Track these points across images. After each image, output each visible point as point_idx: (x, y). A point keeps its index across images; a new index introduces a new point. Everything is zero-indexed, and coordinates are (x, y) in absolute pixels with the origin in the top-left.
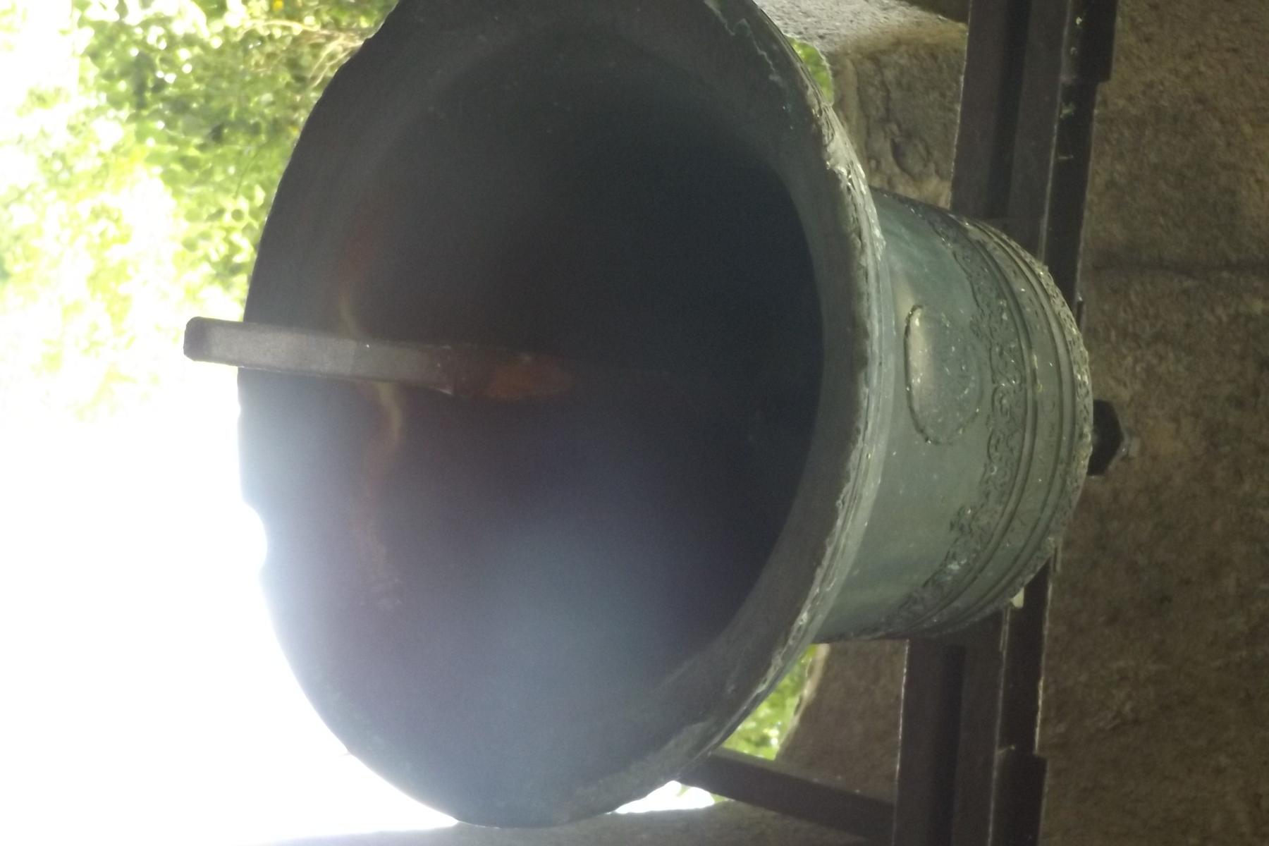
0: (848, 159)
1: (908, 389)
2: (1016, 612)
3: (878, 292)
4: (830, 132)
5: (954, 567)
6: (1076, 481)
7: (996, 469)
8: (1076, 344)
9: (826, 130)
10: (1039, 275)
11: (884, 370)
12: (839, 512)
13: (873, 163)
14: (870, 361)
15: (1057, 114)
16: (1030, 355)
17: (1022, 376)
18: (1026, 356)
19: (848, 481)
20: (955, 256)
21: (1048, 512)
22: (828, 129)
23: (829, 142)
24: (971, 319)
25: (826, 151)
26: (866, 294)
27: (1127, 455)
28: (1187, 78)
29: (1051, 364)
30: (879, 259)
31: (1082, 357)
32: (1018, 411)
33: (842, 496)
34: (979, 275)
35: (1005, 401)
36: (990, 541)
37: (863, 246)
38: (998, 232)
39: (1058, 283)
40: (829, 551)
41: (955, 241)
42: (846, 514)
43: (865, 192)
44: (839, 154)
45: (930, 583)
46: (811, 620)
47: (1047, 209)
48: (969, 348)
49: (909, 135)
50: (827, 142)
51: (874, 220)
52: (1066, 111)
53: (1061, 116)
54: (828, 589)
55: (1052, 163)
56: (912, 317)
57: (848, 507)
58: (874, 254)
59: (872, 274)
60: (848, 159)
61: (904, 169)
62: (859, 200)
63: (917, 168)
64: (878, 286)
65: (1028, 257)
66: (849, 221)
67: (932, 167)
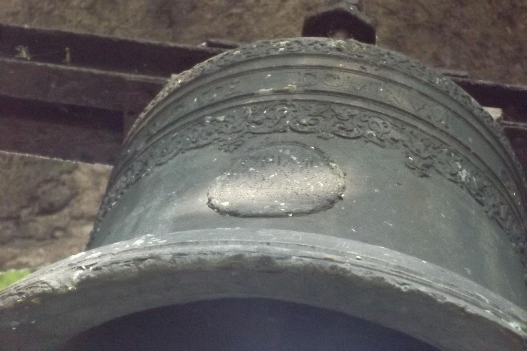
0: (67, 269)
1: (291, 215)
2: (505, 116)
3: (197, 243)
4: (40, 285)
5: (464, 175)
6: (382, 55)
7: (369, 132)
8: (249, 51)
9: (39, 289)
10: (181, 84)
11: (274, 240)
12: (412, 288)
13: (58, 234)
14: (265, 254)
15: (28, 62)
16: (258, 95)
17: (280, 104)
18: (261, 100)
19: (382, 278)
20: (160, 165)
21: (410, 82)
22: (37, 287)
23: (50, 286)
24: (222, 151)
25: (57, 290)
26: (199, 255)
27: (356, 5)
28: (347, 84)
29: (269, 75)
30: (165, 241)
31: (262, 46)
32: (314, 108)
33: (397, 286)
34: (179, 142)
35: (304, 121)
36: (439, 139)
37: (152, 257)
38: (137, 121)
39: (189, 66)
40: (450, 299)
41: (146, 164)
42: (417, 282)
43: (99, 253)
44: (61, 277)
45: (479, 198)
46: (516, 318)
47: (117, 74)
48: (252, 154)
49: (33, 199)
50: (50, 289)
51: (126, 245)
52: (24, 54)
53: (29, 58)
54: (487, 301)
55: (75, 69)
56: (220, 208)
57: (407, 279)
58: (161, 246)
59: (179, 249)
60: (67, 269)
61: (66, 204)
62: (107, 259)
63: (65, 191)
64: (192, 243)
65: (162, 94)
66: (128, 269)
67: (65, 177)
